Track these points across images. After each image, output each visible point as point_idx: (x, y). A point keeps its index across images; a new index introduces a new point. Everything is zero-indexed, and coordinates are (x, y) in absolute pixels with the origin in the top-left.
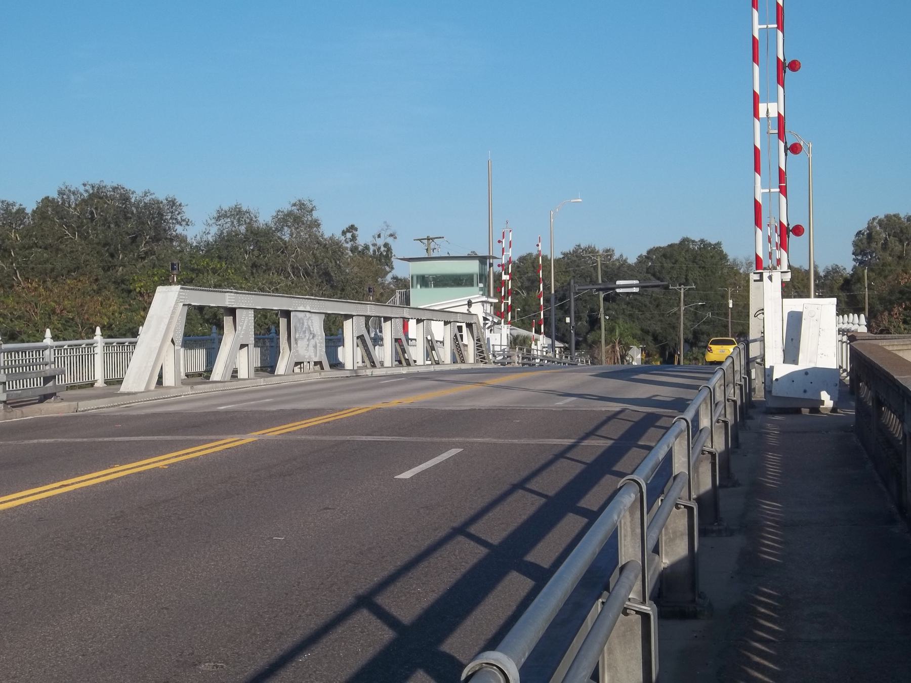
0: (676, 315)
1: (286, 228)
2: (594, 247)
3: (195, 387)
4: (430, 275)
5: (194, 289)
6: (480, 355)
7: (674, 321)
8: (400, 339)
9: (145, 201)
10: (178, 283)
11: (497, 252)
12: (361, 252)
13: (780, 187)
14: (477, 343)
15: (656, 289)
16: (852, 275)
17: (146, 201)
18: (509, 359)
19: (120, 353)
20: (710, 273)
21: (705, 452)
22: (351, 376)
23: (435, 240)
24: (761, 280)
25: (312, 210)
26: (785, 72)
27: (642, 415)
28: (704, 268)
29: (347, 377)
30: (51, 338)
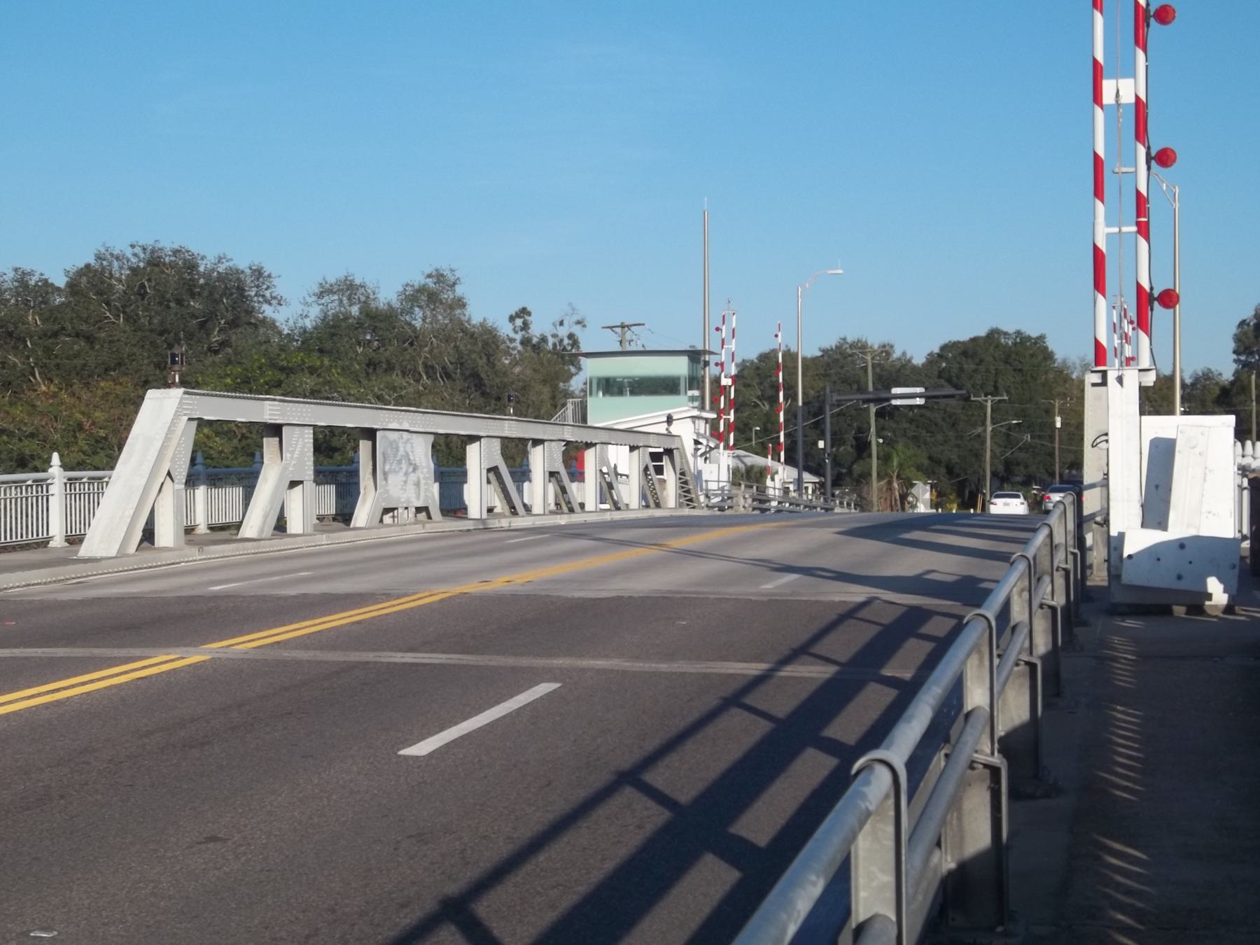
0: (980, 438)
1: (417, 309)
2: (866, 342)
3: (206, 548)
4: (624, 378)
5: (208, 395)
6: (685, 496)
7: (977, 446)
8: (558, 473)
9: (219, 269)
10: (183, 383)
11: (715, 347)
12: (534, 347)
13: (1138, 224)
14: (680, 479)
15: (952, 402)
16: (1232, 383)
17: (220, 270)
18: (730, 501)
19: (94, 494)
20: (1029, 378)
21: (975, 765)
22: (475, 529)
23: (633, 328)
24: (1104, 383)
25: (454, 284)
26: (1148, 26)
27: (899, 612)
28: (1020, 370)
29: (469, 530)
30: (61, 466)
